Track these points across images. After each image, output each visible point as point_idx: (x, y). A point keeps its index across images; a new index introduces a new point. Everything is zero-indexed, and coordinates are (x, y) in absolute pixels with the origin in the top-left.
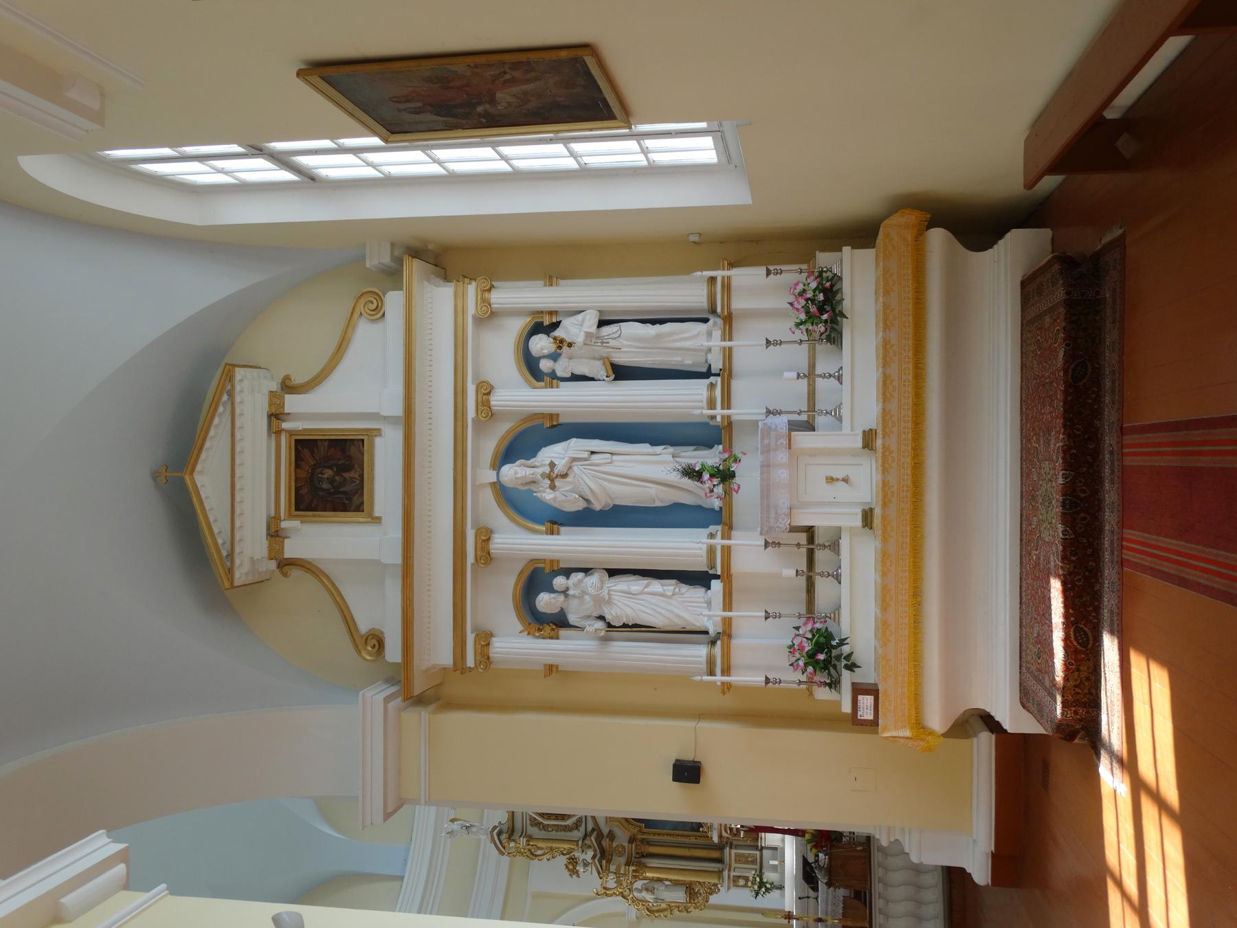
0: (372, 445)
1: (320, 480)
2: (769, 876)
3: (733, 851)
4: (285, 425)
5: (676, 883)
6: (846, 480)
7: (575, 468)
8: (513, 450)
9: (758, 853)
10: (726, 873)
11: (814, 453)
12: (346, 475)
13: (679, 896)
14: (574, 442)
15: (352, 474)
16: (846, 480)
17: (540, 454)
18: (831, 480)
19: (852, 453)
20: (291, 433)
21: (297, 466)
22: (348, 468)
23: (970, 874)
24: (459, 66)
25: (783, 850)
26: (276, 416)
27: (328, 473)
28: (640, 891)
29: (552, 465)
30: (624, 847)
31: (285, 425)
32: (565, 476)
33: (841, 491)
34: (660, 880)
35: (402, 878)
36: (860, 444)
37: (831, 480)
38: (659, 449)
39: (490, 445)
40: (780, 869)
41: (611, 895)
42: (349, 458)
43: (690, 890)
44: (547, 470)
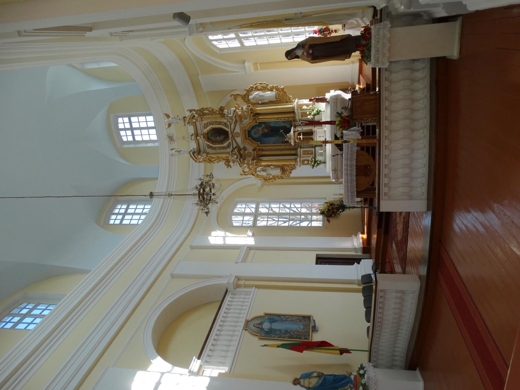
2: (319, 158)
3: (302, 150)
5: (276, 167)
9: (313, 149)
13: (277, 172)
28: (260, 171)
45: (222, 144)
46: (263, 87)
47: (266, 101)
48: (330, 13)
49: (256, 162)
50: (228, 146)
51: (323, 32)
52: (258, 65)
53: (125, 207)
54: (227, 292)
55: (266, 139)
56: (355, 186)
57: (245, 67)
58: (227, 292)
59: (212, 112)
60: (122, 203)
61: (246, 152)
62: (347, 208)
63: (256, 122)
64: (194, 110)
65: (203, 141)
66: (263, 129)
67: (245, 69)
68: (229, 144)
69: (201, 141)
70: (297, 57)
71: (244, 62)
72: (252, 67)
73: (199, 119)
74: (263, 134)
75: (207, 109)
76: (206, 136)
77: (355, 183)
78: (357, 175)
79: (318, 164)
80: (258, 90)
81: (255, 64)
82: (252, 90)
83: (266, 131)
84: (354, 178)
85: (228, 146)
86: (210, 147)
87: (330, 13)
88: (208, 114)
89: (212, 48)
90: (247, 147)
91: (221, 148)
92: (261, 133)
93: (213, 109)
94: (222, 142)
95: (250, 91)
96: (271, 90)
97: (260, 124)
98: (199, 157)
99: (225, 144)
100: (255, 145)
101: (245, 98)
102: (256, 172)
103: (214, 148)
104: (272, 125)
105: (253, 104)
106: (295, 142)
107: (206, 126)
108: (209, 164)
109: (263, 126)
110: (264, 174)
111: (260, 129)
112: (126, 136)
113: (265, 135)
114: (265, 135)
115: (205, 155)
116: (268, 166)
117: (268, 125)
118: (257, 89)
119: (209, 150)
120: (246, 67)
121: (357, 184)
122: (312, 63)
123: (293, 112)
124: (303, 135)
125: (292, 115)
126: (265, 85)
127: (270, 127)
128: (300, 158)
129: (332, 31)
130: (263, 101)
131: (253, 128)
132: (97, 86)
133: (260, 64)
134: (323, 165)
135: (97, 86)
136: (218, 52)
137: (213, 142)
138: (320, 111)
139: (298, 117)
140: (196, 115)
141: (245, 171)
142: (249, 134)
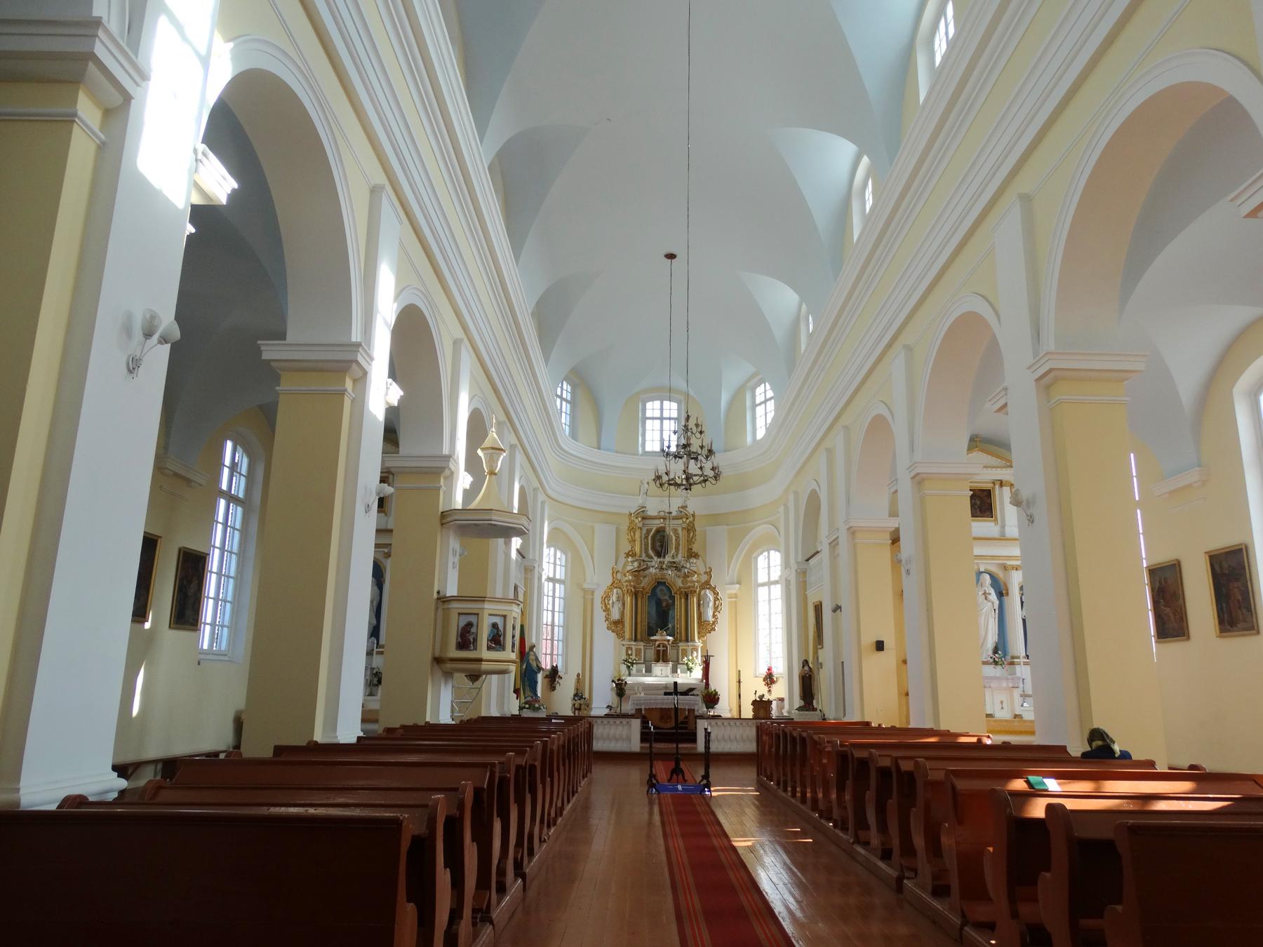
0: (991, 521)
1: (975, 499)
2: (635, 668)
3: (642, 647)
4: (997, 487)
5: (622, 614)
6: (1002, 708)
7: (989, 604)
8: (995, 582)
9: (642, 662)
10: (633, 643)
11: (1011, 695)
12: (978, 510)
13: (615, 615)
14: (998, 602)
15: (979, 513)
16: (1002, 708)
17: (992, 589)
18: (1002, 702)
19: (433, 654)
20: (993, 488)
21: (980, 490)
22: (981, 510)
23: (69, 801)
24: (1181, 601)
25: (651, 676)
26: (1002, 484)
27: (978, 503)
28: (617, 594)
29: (990, 594)
30: (640, 584)
31: (997, 487)
32: (986, 599)
33: (998, 706)
34: (624, 604)
35: (599, 448)
36: (1017, 713)
37: (1002, 702)
38: (997, 636)
39: (993, 569)
40: (639, 673)
41: (613, 576)
42: (985, 512)
43: (616, 623)
44: (987, 592)
45: (651, 548)
46: (718, 606)
47: (702, 609)
48: (175, 602)
49: (631, 591)
50: (648, 556)
51: (770, 678)
52: (734, 599)
53: (569, 399)
54: (524, 557)
55: (654, 603)
56: (651, 707)
57: (733, 584)
58: (524, 557)
59: (690, 541)
60: (573, 393)
61: (642, 578)
62: (621, 699)
63: (675, 593)
64: (694, 520)
65: (657, 524)
66: (667, 600)
67: (730, 584)
68: (652, 558)
69: (657, 522)
70: (803, 667)
71: (739, 583)
72: (734, 592)
73: (685, 525)
74: (660, 600)
75: (694, 535)
76: (662, 529)
77: (654, 707)
78: (661, 709)
79: (628, 667)
80: (715, 601)
81: (736, 596)
82: (715, 593)
83: (664, 604)
84: (659, 706)
85: (648, 556)
86: (648, 531)
87: (175, 602)
88: (688, 537)
89: (760, 550)
90: (647, 579)
91: (646, 545)
92: (662, 598)
93: (694, 543)
94: (653, 548)
95: (713, 590)
96: (714, 616)
97: (673, 598)
98: (640, 519)
99: (651, 552)
100: (649, 589)
101: (707, 585)
102: (616, 587)
103: (646, 537)
104: (671, 612)
105: (699, 594)
106: (656, 640)
107: (675, 531)
108: (627, 528)
109: (671, 601)
110: (614, 598)
111: (667, 597)
112: (652, 408)
113: (659, 602)
114: (659, 602)
115: (640, 525)
116: (624, 604)
117: (671, 608)
118: (716, 599)
119: (644, 531)
120: (735, 586)
121: (653, 709)
122: (799, 676)
123: (687, 641)
124: (663, 651)
125: (683, 638)
126: (719, 609)
127: (669, 609)
128: (635, 645)
129: (770, 687)
130: (701, 606)
131: (669, 589)
132: (725, 398)
133: (736, 602)
134: (627, 672)
135: (725, 398)
136: (754, 555)
137: (653, 538)
138: (691, 672)
139: (682, 645)
140: (688, 521)
141: (618, 574)
142: (661, 583)
